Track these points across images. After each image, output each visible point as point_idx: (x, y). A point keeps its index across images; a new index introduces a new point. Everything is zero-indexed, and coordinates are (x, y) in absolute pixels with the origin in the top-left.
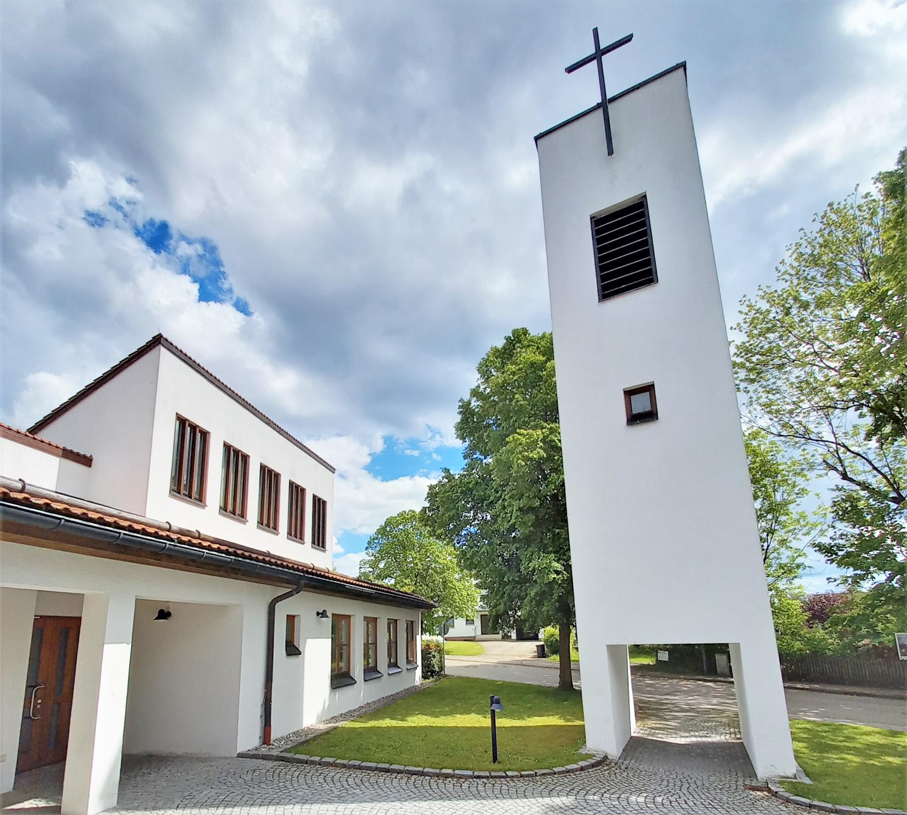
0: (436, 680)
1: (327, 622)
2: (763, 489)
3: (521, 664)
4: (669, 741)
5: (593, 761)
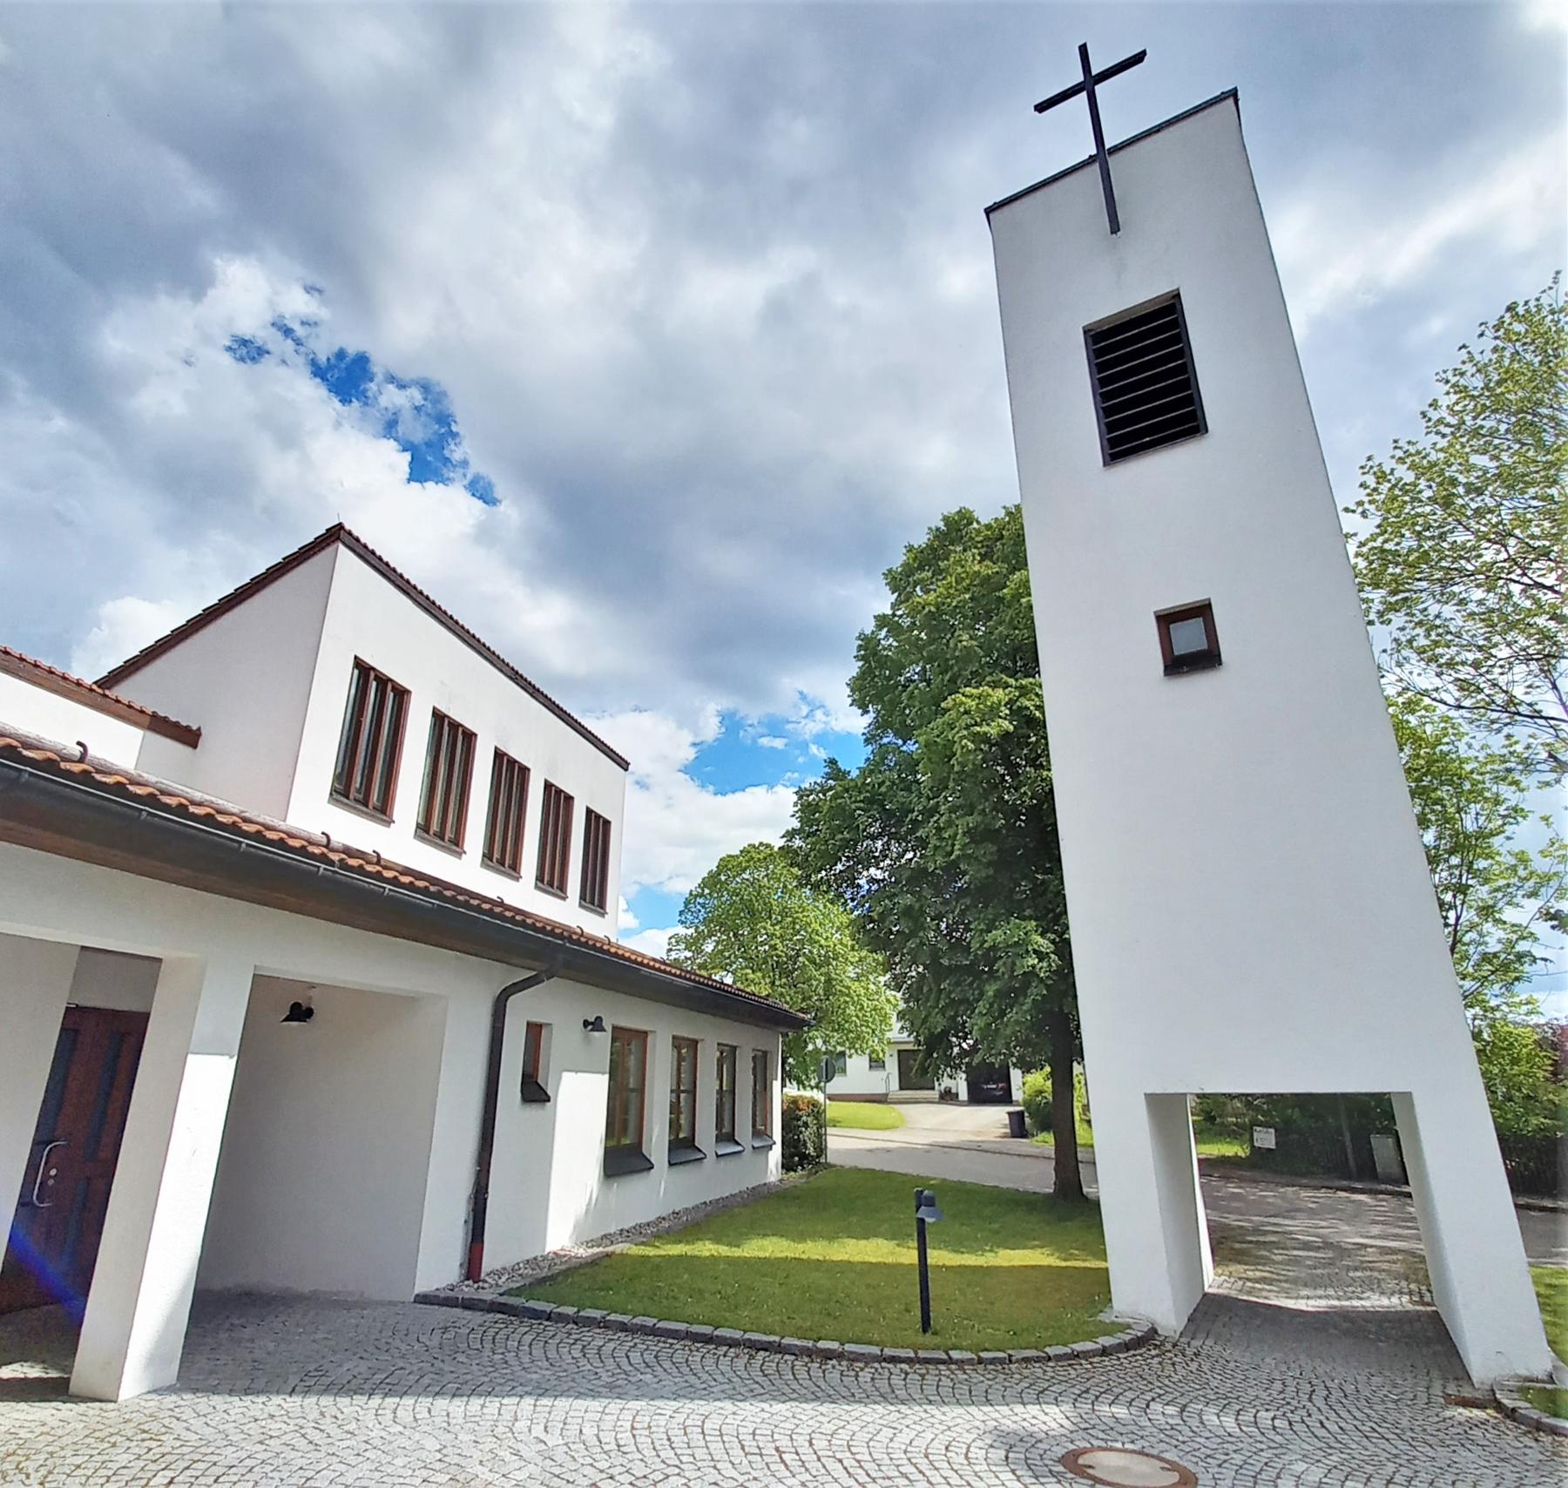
0: (810, 1175)
1: (603, 1039)
2: (1439, 808)
3: (979, 1149)
4: (1283, 1305)
5: (1128, 1338)
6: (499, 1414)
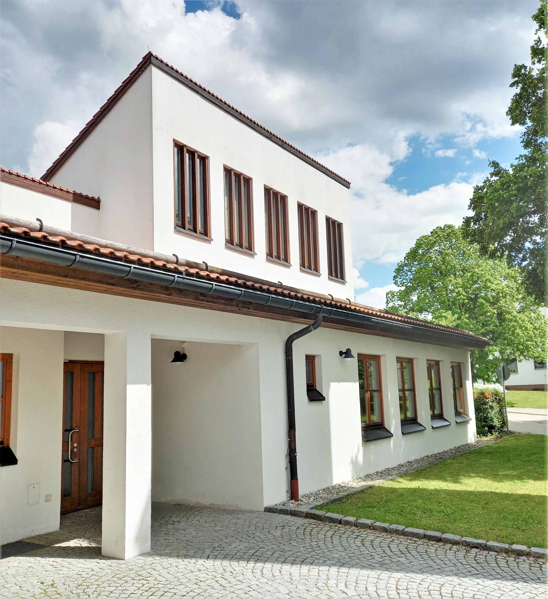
1: (353, 363)
6: (319, 576)
